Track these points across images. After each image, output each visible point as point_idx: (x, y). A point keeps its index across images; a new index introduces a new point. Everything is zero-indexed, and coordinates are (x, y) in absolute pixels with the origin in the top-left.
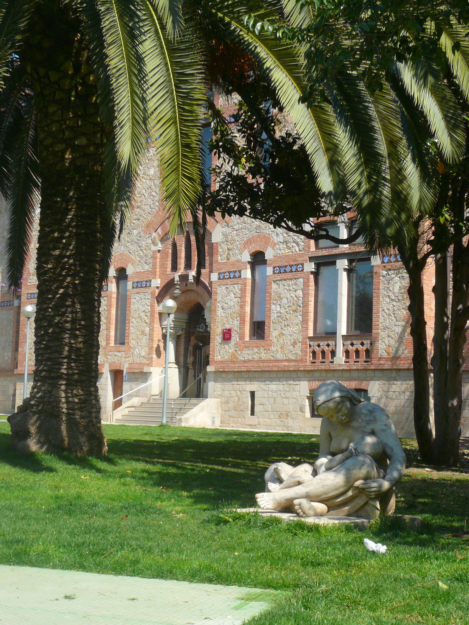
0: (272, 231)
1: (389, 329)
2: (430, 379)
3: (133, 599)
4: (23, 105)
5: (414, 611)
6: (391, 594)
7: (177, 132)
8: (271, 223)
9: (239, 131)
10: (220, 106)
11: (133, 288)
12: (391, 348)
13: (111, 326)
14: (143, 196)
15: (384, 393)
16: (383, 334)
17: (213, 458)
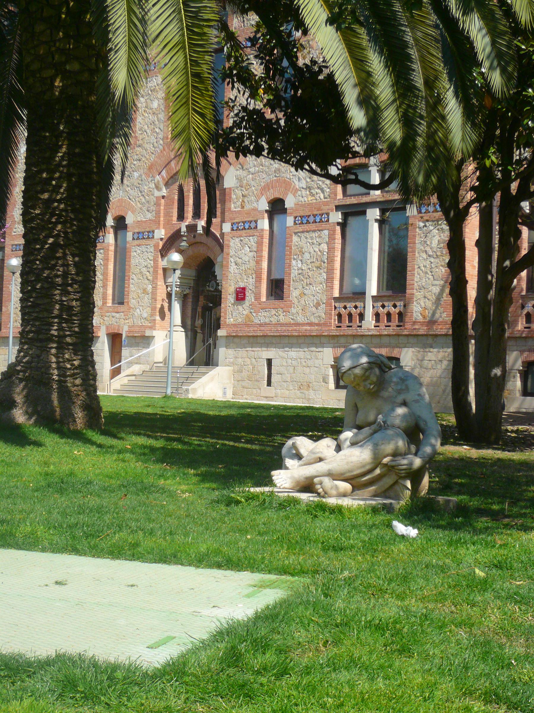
0: (293, 175)
1: (426, 289)
2: (470, 346)
3: (132, 586)
4: (6, 23)
5: (447, 600)
6: (421, 582)
7: (186, 60)
8: (292, 165)
9: (256, 57)
10: (235, 28)
11: (133, 239)
12: (427, 311)
13: (108, 283)
14: (145, 133)
15: (418, 362)
16: (418, 295)
17: (224, 433)
